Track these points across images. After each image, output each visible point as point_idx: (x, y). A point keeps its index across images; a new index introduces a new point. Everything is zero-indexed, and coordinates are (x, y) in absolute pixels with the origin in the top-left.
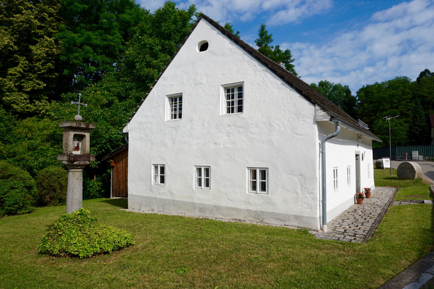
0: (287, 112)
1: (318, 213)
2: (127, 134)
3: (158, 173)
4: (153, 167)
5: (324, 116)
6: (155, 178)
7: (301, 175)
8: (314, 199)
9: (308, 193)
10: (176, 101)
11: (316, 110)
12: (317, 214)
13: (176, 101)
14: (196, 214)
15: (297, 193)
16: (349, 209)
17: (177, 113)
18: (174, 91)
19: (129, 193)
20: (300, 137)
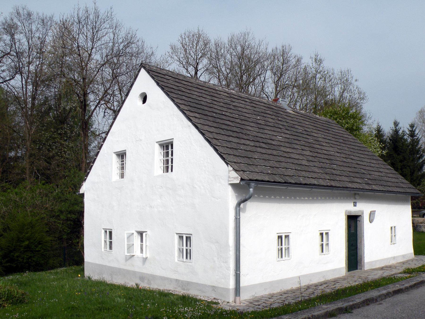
0: (207, 172)
1: (232, 285)
2: (83, 195)
3: (107, 239)
4: (103, 231)
5: (235, 178)
6: (183, 92)
7: (218, 242)
8: (228, 268)
9: (223, 262)
10: (122, 155)
11: (229, 171)
12: (230, 285)
13: (122, 155)
14: (131, 283)
15: (214, 261)
16: (318, 283)
17: (144, 101)
18: (120, 149)
19: (85, 260)
20: (217, 200)
